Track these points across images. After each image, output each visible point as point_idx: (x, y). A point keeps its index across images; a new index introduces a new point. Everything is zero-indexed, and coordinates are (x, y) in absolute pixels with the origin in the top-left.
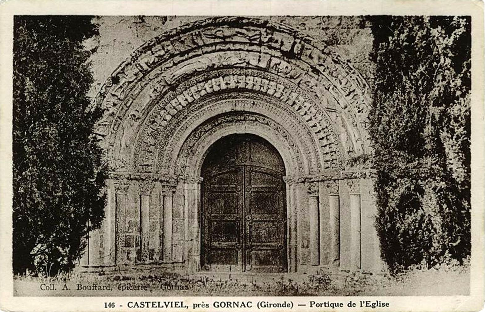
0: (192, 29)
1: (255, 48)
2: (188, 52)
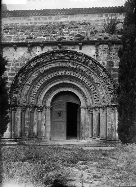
0: (50, 54)
1: (72, 61)
2: (48, 62)
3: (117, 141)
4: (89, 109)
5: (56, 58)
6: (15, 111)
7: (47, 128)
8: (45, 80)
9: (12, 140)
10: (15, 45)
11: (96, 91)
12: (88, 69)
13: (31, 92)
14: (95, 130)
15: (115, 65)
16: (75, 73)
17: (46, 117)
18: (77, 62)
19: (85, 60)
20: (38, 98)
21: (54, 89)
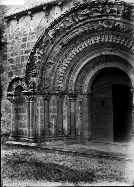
1: (105, 18)
3: (17, 125)
5: (81, 18)
6: (34, 100)
7: (85, 123)
8: (73, 54)
9: (30, 140)
10: (29, 13)
13: (56, 73)
17: (83, 107)
20: (68, 81)
21: (91, 66)
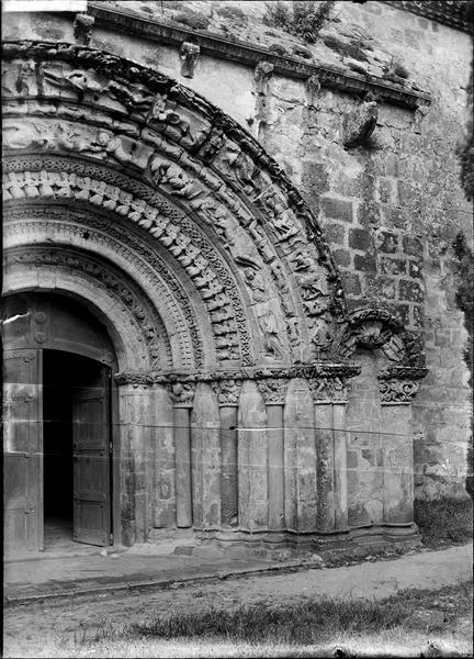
1: (132, 128)
4: (178, 387)
5: (50, 92)
11: (225, 299)
12: (209, 185)
14: (212, 490)
15: (332, 185)
16: (130, 196)
18: (158, 140)
19: (208, 136)
